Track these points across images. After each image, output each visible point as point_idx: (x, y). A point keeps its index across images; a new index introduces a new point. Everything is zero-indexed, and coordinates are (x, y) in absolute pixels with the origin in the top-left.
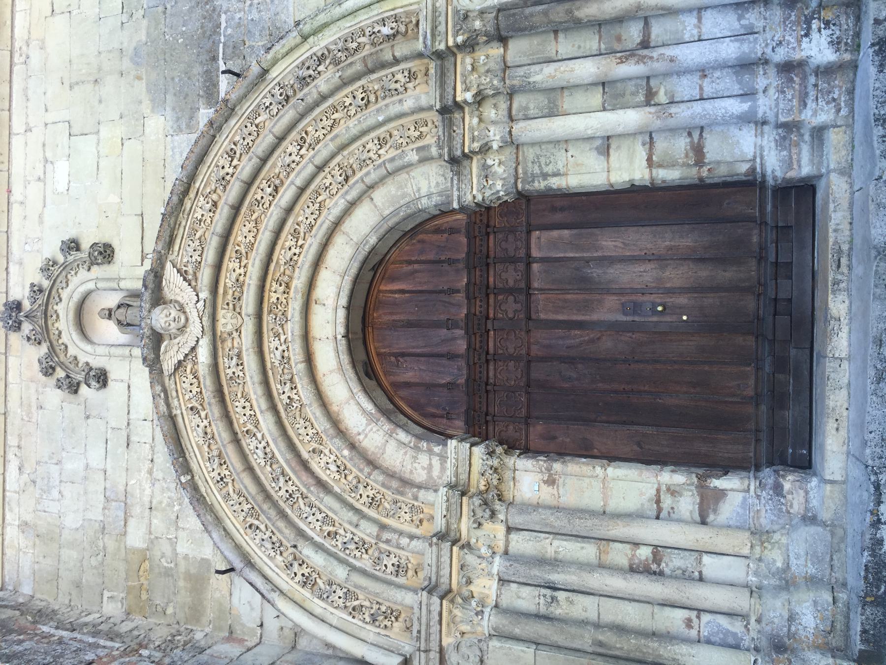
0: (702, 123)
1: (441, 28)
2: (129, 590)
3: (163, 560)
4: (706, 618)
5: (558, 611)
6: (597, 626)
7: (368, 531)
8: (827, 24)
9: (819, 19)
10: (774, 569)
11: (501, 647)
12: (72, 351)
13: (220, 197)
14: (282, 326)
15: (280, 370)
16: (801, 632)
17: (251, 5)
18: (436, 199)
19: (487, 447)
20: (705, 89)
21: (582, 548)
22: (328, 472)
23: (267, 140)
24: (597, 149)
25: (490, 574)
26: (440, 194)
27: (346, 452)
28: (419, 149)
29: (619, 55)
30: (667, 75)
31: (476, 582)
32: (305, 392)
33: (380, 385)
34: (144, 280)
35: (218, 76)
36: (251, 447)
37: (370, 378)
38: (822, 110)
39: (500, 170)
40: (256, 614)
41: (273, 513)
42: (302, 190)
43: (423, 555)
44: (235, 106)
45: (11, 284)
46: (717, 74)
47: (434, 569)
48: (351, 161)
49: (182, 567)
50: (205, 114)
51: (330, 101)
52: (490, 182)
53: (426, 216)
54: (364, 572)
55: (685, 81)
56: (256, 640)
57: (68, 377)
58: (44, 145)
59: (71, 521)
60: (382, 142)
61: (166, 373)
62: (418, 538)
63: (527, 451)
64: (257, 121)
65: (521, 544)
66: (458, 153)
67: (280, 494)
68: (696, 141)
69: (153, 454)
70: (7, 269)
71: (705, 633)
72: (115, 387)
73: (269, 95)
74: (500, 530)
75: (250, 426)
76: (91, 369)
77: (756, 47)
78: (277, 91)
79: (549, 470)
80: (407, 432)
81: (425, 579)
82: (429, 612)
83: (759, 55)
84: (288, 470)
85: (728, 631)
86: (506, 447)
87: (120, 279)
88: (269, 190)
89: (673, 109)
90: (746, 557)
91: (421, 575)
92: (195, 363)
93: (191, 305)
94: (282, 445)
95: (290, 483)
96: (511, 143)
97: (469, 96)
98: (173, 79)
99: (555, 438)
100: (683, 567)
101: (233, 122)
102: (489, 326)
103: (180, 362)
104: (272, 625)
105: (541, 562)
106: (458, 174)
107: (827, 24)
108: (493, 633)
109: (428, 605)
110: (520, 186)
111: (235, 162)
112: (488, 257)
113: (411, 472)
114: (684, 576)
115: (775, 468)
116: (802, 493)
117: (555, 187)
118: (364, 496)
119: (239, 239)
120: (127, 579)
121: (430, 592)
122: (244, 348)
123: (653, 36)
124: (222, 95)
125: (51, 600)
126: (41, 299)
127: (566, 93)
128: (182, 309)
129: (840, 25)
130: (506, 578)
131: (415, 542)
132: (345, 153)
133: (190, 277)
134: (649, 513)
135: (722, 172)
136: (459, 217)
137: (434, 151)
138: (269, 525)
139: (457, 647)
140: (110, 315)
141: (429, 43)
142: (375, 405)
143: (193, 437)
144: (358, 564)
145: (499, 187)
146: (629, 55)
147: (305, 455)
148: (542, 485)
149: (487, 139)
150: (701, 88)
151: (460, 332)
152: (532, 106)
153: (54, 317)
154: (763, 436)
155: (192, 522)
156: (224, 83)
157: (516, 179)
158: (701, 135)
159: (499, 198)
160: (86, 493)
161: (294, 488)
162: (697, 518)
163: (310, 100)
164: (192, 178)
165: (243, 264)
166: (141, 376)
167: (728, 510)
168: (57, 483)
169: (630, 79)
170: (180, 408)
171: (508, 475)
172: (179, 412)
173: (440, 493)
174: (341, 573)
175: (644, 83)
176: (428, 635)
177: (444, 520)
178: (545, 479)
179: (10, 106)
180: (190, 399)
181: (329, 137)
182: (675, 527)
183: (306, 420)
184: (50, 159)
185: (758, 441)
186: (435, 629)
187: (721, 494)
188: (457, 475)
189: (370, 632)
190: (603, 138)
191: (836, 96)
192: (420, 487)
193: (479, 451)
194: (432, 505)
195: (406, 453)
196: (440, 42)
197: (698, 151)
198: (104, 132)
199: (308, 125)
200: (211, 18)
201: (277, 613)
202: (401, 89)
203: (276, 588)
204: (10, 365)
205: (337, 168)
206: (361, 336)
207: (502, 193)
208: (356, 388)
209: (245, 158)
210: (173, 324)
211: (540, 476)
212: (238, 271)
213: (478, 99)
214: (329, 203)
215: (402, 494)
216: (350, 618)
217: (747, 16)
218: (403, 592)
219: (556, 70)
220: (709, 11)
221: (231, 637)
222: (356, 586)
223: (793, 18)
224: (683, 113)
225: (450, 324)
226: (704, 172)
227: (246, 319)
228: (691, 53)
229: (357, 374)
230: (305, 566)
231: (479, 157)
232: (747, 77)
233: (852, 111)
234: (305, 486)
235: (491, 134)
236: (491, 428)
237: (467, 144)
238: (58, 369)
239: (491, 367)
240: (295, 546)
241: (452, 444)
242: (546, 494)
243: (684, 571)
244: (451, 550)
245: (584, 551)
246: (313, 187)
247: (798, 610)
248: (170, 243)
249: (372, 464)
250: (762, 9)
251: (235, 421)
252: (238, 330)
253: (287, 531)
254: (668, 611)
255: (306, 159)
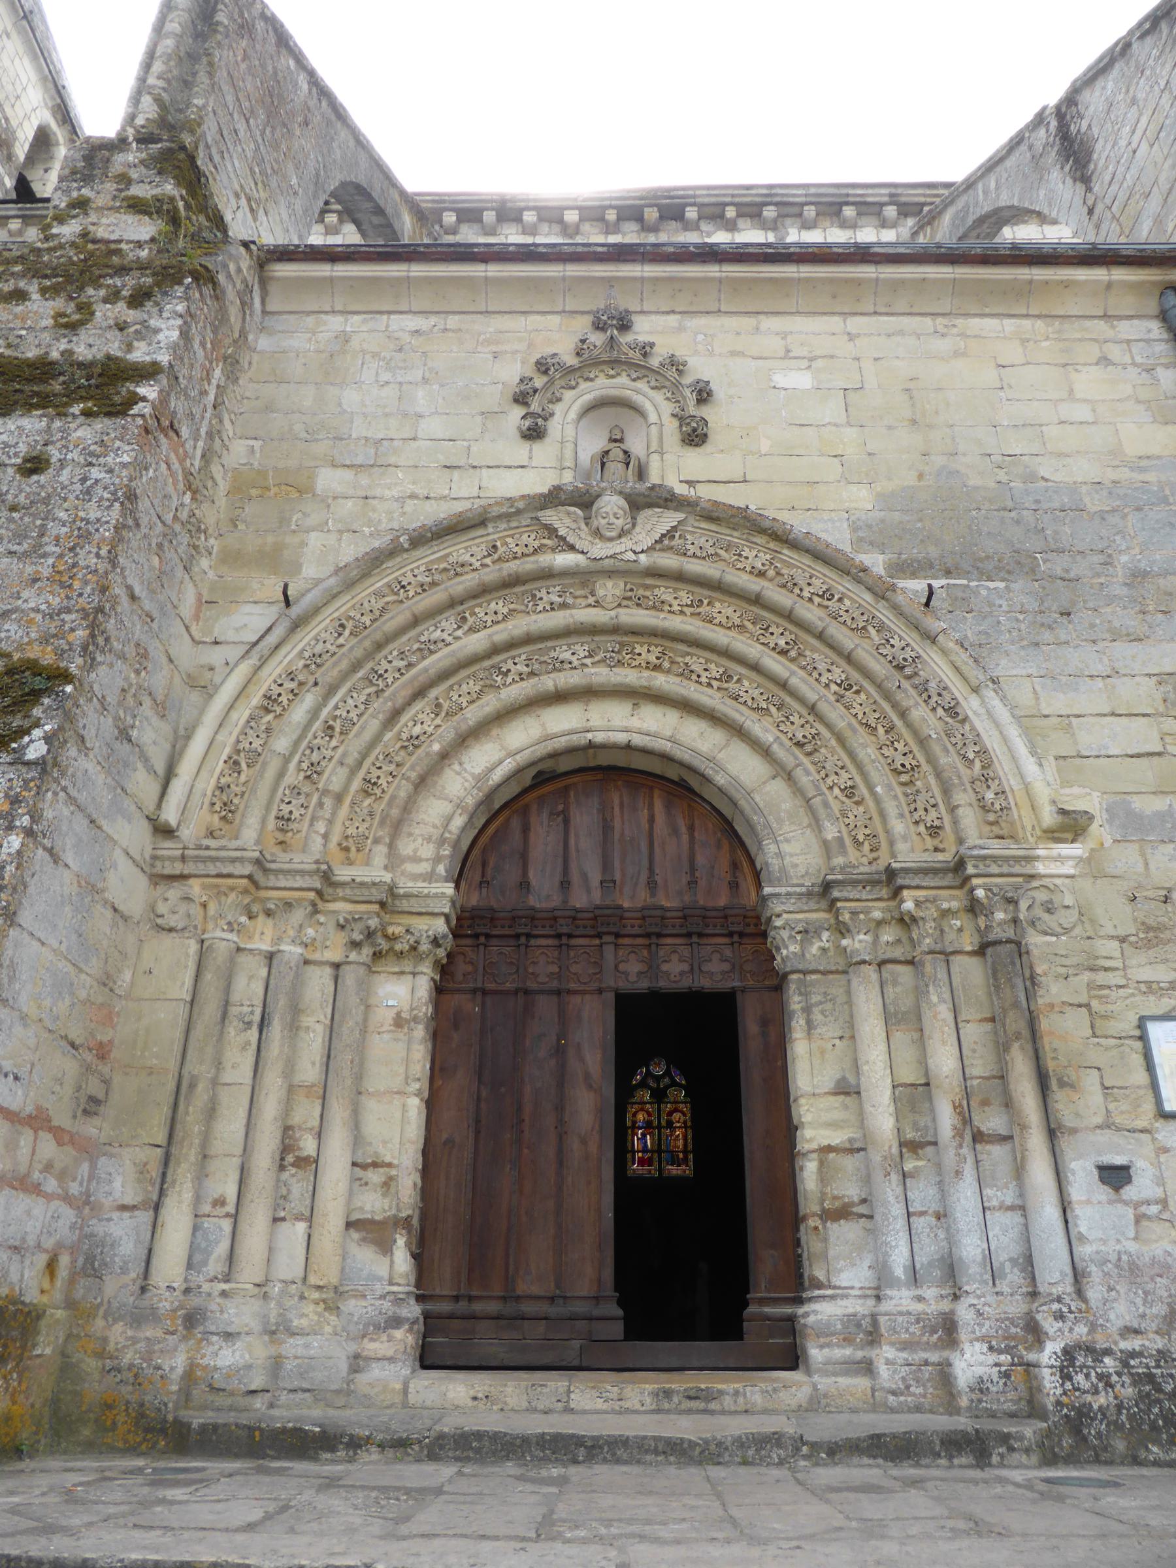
0: (877, 1217)
1: (994, 869)
2: (262, 473)
3: (299, 515)
4: (227, 1225)
5: (231, 1031)
6: (215, 1083)
7: (334, 779)
8: (1006, 1375)
9: (1013, 1364)
10: (290, 1315)
11: (187, 955)
12: (568, 395)
13: (771, 580)
14: (603, 661)
15: (545, 658)
16: (211, 1349)
17: (1017, 620)
18: (775, 864)
19: (445, 936)
20: (922, 1219)
21: (313, 1064)
22: (411, 724)
23: (847, 640)
24: (844, 1079)
25: (278, 940)
26: (783, 869)
27: (436, 747)
28: (840, 840)
29: (965, 1103)
30: (939, 1166)
31: (270, 922)
32: (514, 692)
33: (525, 791)
34: (660, 486)
35: (925, 578)
36: (443, 624)
37: (534, 777)
38: (895, 1372)
39: (814, 949)
40: (231, 636)
41: (359, 653)
42: (784, 685)
43: (304, 851)
44: (887, 600)
45: (653, 317)
46: (942, 1235)
47: (286, 866)
48: (823, 750)
49: (290, 540)
50: (876, 562)
51: (898, 723)
52: (799, 937)
53: (753, 850)
54: (281, 774)
55: (932, 1191)
56: (197, 635)
57: (535, 391)
58: (832, 357)
59: (351, 397)
60: (849, 791)
61: (540, 514)
62: (325, 845)
63: (440, 990)
64: (870, 628)
65: (318, 982)
66: (836, 894)
67: (384, 662)
68: (855, 1210)
69: (435, 499)
70: (673, 312)
71: (207, 1223)
72: (521, 451)
73: (903, 643)
74: (334, 954)
75: (471, 620)
76: (546, 419)
77: (973, 1281)
78: (908, 654)
79: (415, 1019)
80: (464, 829)
81: (272, 854)
82: (233, 860)
83: (966, 1288)
84: (414, 671)
85: (209, 1254)
86: (444, 961)
87: (662, 454)
88: (782, 642)
89: (895, 1178)
90: (305, 1279)
91: (277, 850)
92: (553, 550)
93: (629, 545)
94: (446, 663)
95: (397, 675)
96: (850, 965)
97: (909, 905)
98: (921, 520)
99: (456, 1026)
100: (291, 1197)
101: (868, 597)
102: (606, 939)
103: (556, 530)
104: (216, 656)
105: (296, 1010)
106: (809, 894)
107: (1006, 1375)
108: (206, 944)
109: (240, 860)
110: (794, 977)
111: (817, 600)
112: (700, 935)
113: (410, 834)
114: (281, 1198)
115: (422, 1319)
116: (390, 1353)
117: (793, 1023)
118: (379, 772)
119: (717, 604)
120: (276, 469)
121: (258, 862)
122: (574, 611)
123: (989, 1147)
124: (901, 584)
125: (249, 374)
126: (635, 356)
127: (916, 1035)
128: (622, 533)
129: (1004, 1392)
130: (275, 962)
131: (319, 840)
132: (833, 742)
133: (666, 542)
134: (360, 1153)
135: (810, 1243)
136: (753, 894)
137: (839, 860)
138: (344, 649)
139: (188, 899)
140: (616, 441)
141: (975, 852)
142: (499, 786)
143: (460, 550)
144: (292, 766)
145: (792, 948)
146: (965, 1118)
147: (433, 693)
148: (395, 1011)
149: (855, 931)
150: (922, 1213)
151: (597, 897)
152: (898, 989)
153: (612, 372)
154: (462, 1307)
155: (350, 551)
156: (917, 586)
157: (805, 973)
158: (862, 1216)
159: (778, 949)
160: (386, 415)
161: (390, 681)
162: (355, 1216)
163: (899, 696)
164: (794, 545)
165: (685, 609)
166: (536, 483)
167: (366, 1258)
168: (400, 379)
169: (934, 1120)
170: (492, 533)
171: (408, 966)
172: (490, 530)
173: (383, 873)
174: (281, 744)
175: (929, 1139)
176: (204, 860)
177: (348, 879)
178: (404, 1015)
179: (881, 314)
180: (507, 544)
181: (853, 721)
182: (343, 1187)
183: (480, 693)
184: (814, 364)
185: (457, 1298)
186: (212, 869)
187: (385, 1247)
188: (407, 896)
189: (207, 784)
190: (858, 1086)
191: (912, 1389)
192: (391, 846)
193: (440, 926)
194: (367, 863)
195: (435, 826)
196: (975, 866)
197: (842, 1213)
198: (851, 433)
199: (869, 695)
200: (999, 569)
201: (232, 661)
202: (916, 816)
203: (263, 661)
204: (549, 317)
205: (813, 731)
206: (592, 764)
207: (784, 952)
208: (522, 758)
209: (821, 613)
210: (603, 522)
211: (406, 1007)
212: (675, 603)
213: (906, 918)
214: (767, 722)
215: (382, 823)
216: (224, 757)
217: (1016, 1270)
218: (257, 826)
219: (944, 1020)
220: (1022, 1220)
221: (205, 603)
222: (265, 764)
223: (1013, 1330)
224: (889, 1192)
225: (608, 884)
226: (812, 1222)
227: (613, 613)
228: (966, 1198)
229: (541, 760)
230: (291, 697)
231: (833, 921)
232: (937, 1273)
233: (893, 1410)
234: (394, 694)
235: (862, 937)
236: (468, 941)
237: (848, 904)
238: (545, 379)
239: (550, 942)
240: (316, 684)
241: (449, 889)
242: (383, 1016)
243: (285, 1198)
244: (309, 889)
245: (310, 1066)
246: (788, 699)
247: (238, 1344)
248: (710, 518)
249: (423, 782)
250: (1024, 1290)
251: (479, 601)
252: (597, 604)
253: (335, 672)
254: (234, 1176)
255: (824, 691)
